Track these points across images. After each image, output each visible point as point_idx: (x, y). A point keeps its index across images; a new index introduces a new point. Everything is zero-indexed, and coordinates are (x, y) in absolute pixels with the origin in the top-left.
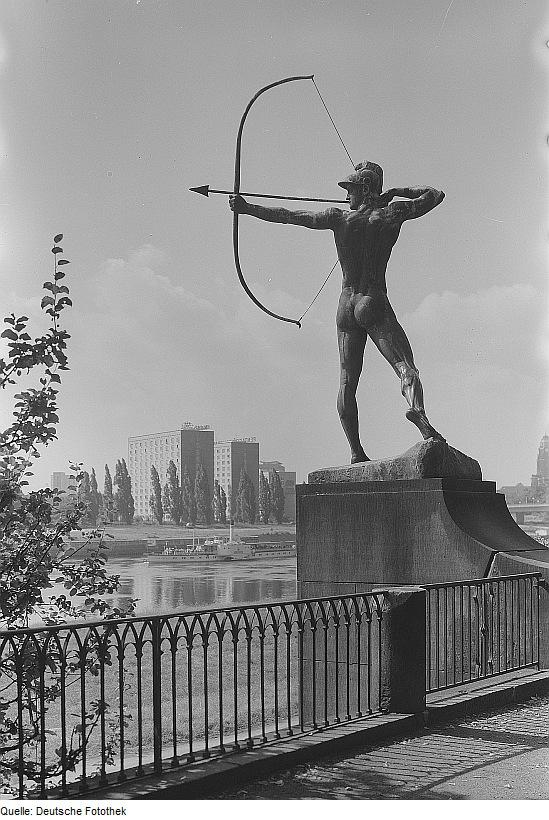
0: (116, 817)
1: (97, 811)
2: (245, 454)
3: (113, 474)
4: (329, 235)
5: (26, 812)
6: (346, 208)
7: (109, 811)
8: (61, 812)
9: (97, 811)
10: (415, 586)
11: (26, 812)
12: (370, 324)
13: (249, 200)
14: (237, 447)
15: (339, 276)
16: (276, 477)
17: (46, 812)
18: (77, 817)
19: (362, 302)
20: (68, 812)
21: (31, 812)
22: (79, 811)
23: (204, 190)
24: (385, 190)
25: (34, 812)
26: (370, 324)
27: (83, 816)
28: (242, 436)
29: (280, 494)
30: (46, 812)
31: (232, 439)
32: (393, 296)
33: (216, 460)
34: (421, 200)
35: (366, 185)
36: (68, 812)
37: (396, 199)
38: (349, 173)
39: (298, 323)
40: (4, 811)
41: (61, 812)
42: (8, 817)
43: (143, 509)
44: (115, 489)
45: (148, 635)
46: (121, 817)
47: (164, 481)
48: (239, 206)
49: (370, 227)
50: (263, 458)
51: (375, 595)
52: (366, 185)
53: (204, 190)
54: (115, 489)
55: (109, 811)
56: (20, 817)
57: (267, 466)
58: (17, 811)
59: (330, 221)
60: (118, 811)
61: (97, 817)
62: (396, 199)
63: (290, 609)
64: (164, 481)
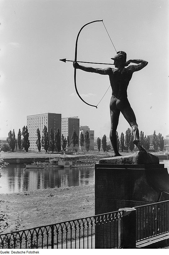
0: (36, 254)
1: (30, 252)
2: (74, 123)
3: (22, 131)
4: (107, 77)
5: (8, 252)
6: (113, 67)
7: (34, 252)
8: (19, 253)
9: (30, 252)
10: (137, 184)
11: (8, 252)
12: (121, 107)
13: (80, 64)
14: (70, 120)
15: (110, 90)
16: (87, 133)
17: (14, 252)
18: (24, 254)
19: (118, 101)
20: (21, 253)
21: (10, 253)
22: (25, 252)
23: (64, 60)
24: (127, 60)
25: (10, 252)
26: (121, 107)
27: (26, 254)
28: (73, 116)
29: (88, 141)
30: (14, 252)
31: (69, 117)
32: (129, 98)
33: (62, 123)
34: (140, 65)
35: (121, 59)
36: (21, 253)
37: (131, 64)
38: (115, 55)
39: (96, 107)
40: (1, 252)
41: (19, 253)
42: (2, 254)
43: (33, 146)
44: (22, 137)
45: (50, 230)
46: (38, 254)
47: (42, 134)
48: (76, 66)
49: (121, 74)
50: (82, 124)
51: (119, 212)
52: (121, 59)
53: (64, 60)
54: (22, 137)
55: (34, 252)
56: (6, 254)
57: (83, 128)
58: (5, 252)
59: (108, 72)
60: (37, 252)
61: (30, 254)
62: (131, 64)
63: (92, 218)
64: (42, 134)
